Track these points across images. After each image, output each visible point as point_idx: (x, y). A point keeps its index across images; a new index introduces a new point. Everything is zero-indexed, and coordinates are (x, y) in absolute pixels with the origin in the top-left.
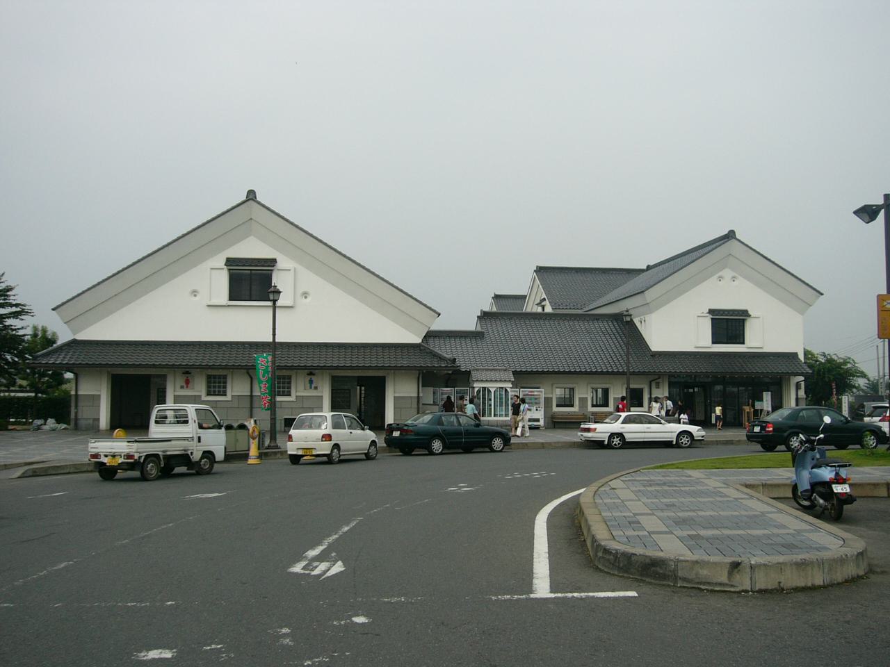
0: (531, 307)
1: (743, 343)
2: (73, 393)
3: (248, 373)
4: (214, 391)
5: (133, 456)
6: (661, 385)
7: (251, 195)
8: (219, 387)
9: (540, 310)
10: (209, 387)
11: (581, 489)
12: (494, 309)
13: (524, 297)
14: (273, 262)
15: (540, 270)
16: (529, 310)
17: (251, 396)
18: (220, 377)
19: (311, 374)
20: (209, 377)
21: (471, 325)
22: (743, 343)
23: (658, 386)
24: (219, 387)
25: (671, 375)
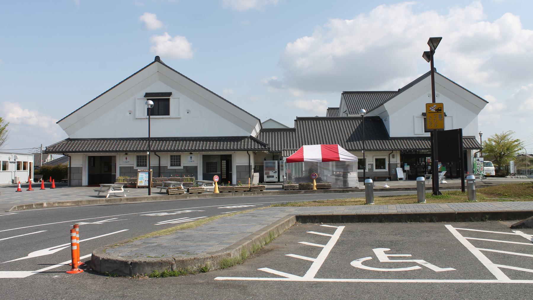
0: (342, 115)
1: (169, 115)
2: (69, 166)
3: (155, 154)
4: (177, 164)
5: (42, 204)
6: (395, 156)
7: (157, 59)
8: (177, 162)
9: (346, 116)
10: (138, 162)
11: (23, 270)
12: (328, 116)
13: (338, 109)
14: (170, 94)
15: (345, 93)
16: (341, 116)
17: (159, 167)
18: (177, 156)
19: (127, 154)
20: (138, 157)
21: (291, 125)
22: (169, 115)
23: (393, 157)
24: (177, 162)
25: (401, 150)
